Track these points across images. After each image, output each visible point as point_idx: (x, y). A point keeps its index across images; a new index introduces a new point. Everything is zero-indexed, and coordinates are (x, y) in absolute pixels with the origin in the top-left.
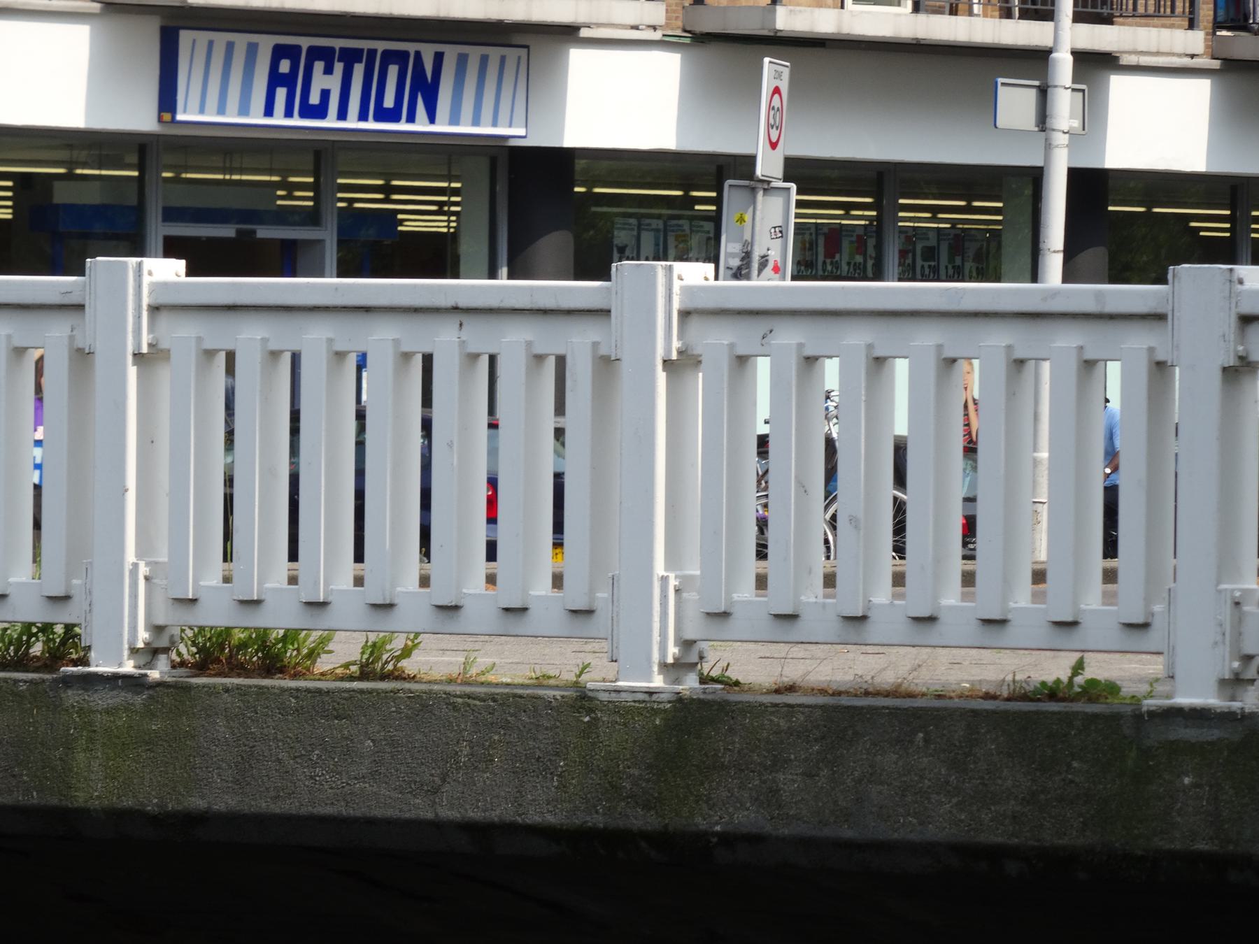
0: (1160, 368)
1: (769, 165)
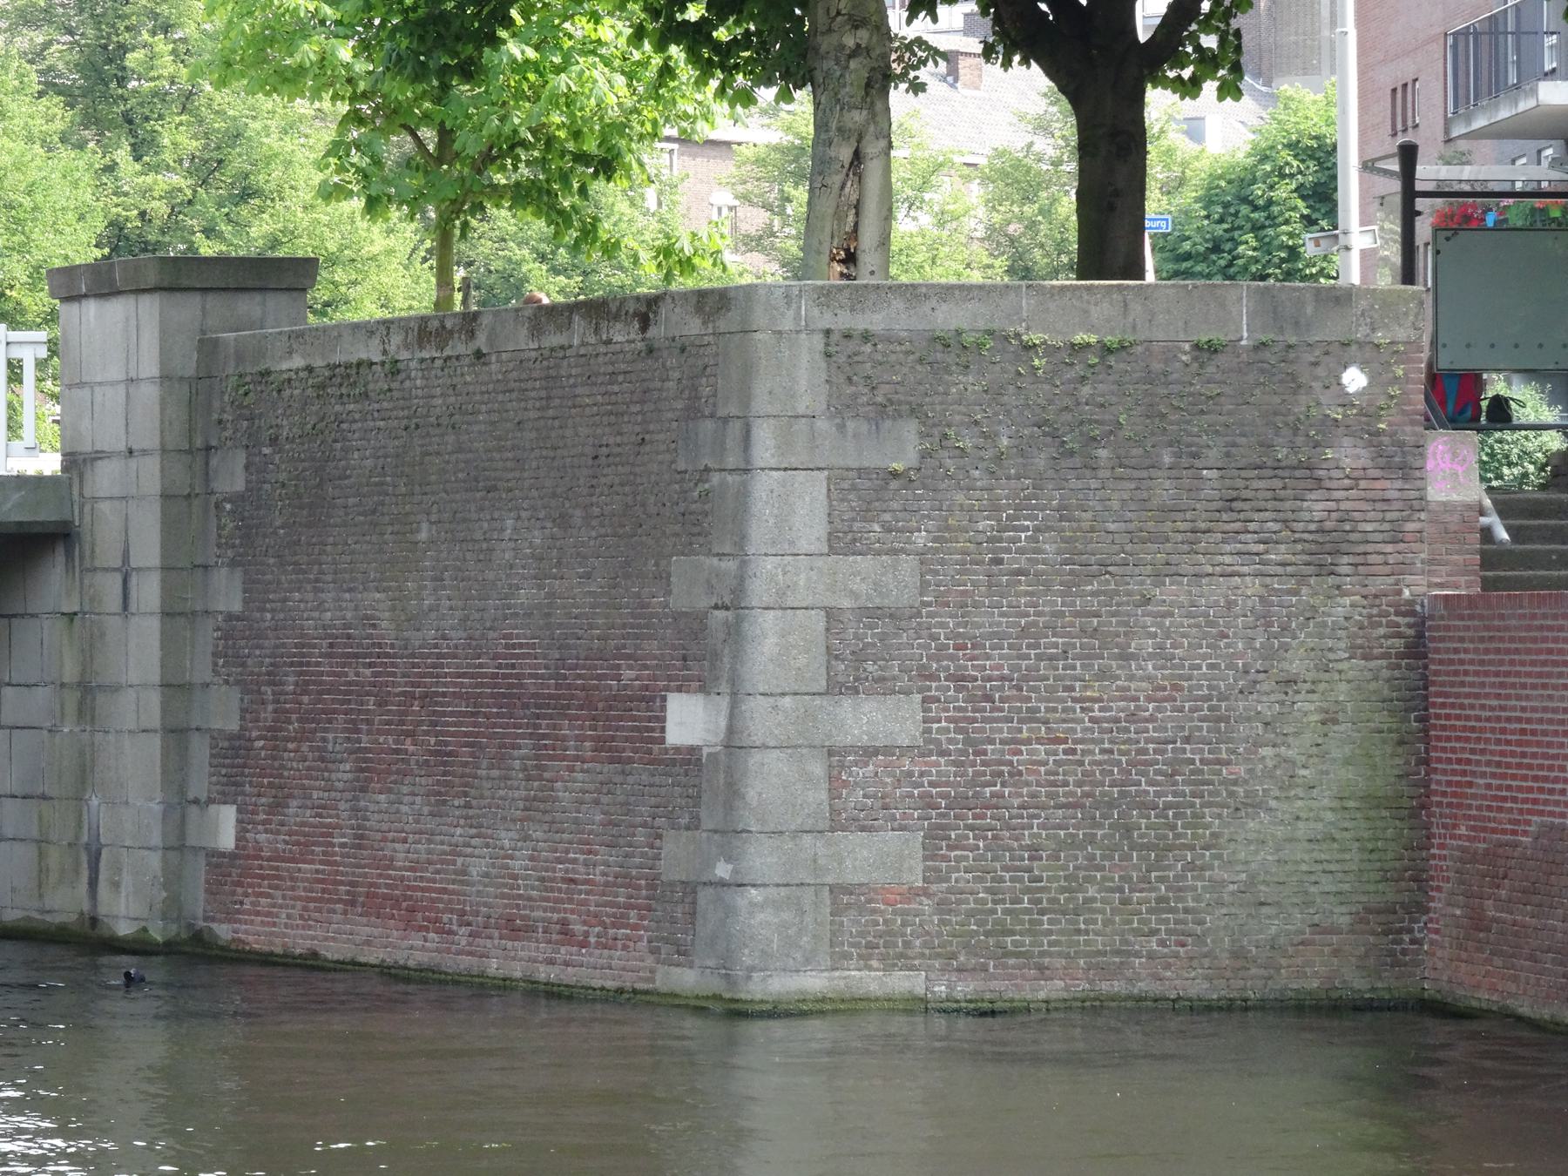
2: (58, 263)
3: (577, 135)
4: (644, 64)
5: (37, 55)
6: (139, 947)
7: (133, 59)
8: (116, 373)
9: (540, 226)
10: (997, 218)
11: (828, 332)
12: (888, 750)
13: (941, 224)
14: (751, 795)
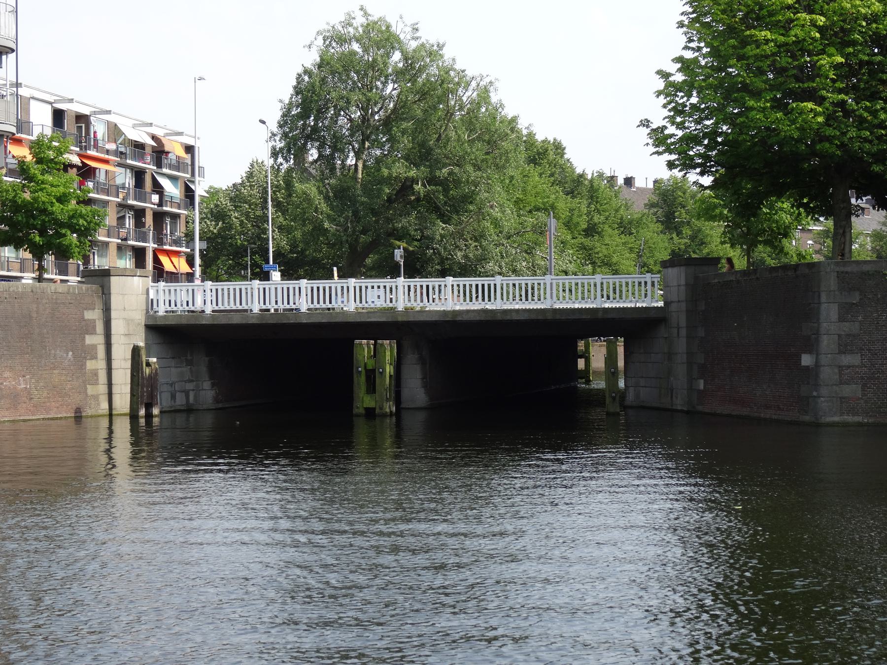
2: (660, 260)
3: (778, 229)
4: (794, 212)
5: (655, 214)
6: (682, 411)
7: (677, 214)
8: (675, 284)
9: (769, 249)
10: (874, 245)
11: (838, 272)
12: (853, 366)
13: (860, 247)
14: (821, 377)
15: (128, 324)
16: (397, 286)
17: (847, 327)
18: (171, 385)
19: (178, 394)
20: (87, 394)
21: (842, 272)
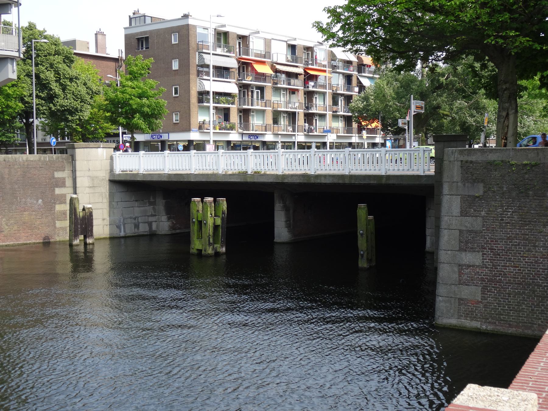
0: (380, 154)
1: (280, 142)
11: (462, 161)
12: (473, 266)
15: (93, 180)
16: (247, 155)
17: (469, 223)
18: (135, 219)
19: (141, 225)
20: (55, 227)
21: (467, 162)
